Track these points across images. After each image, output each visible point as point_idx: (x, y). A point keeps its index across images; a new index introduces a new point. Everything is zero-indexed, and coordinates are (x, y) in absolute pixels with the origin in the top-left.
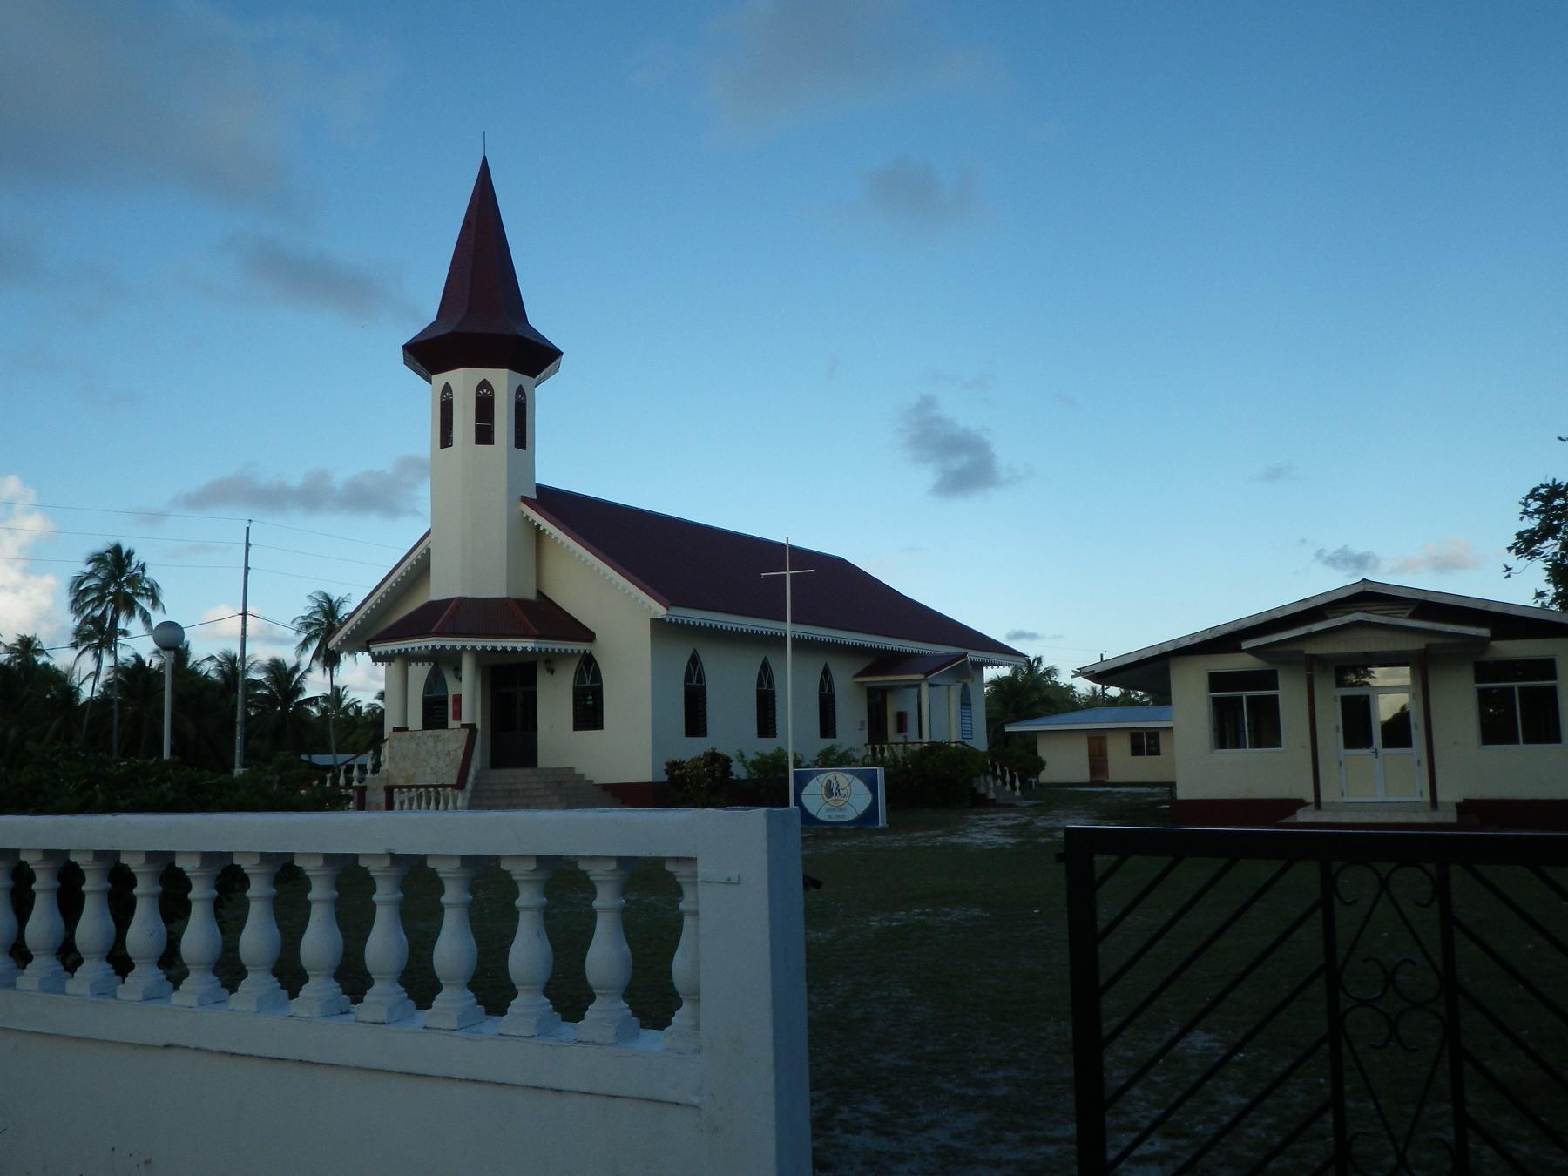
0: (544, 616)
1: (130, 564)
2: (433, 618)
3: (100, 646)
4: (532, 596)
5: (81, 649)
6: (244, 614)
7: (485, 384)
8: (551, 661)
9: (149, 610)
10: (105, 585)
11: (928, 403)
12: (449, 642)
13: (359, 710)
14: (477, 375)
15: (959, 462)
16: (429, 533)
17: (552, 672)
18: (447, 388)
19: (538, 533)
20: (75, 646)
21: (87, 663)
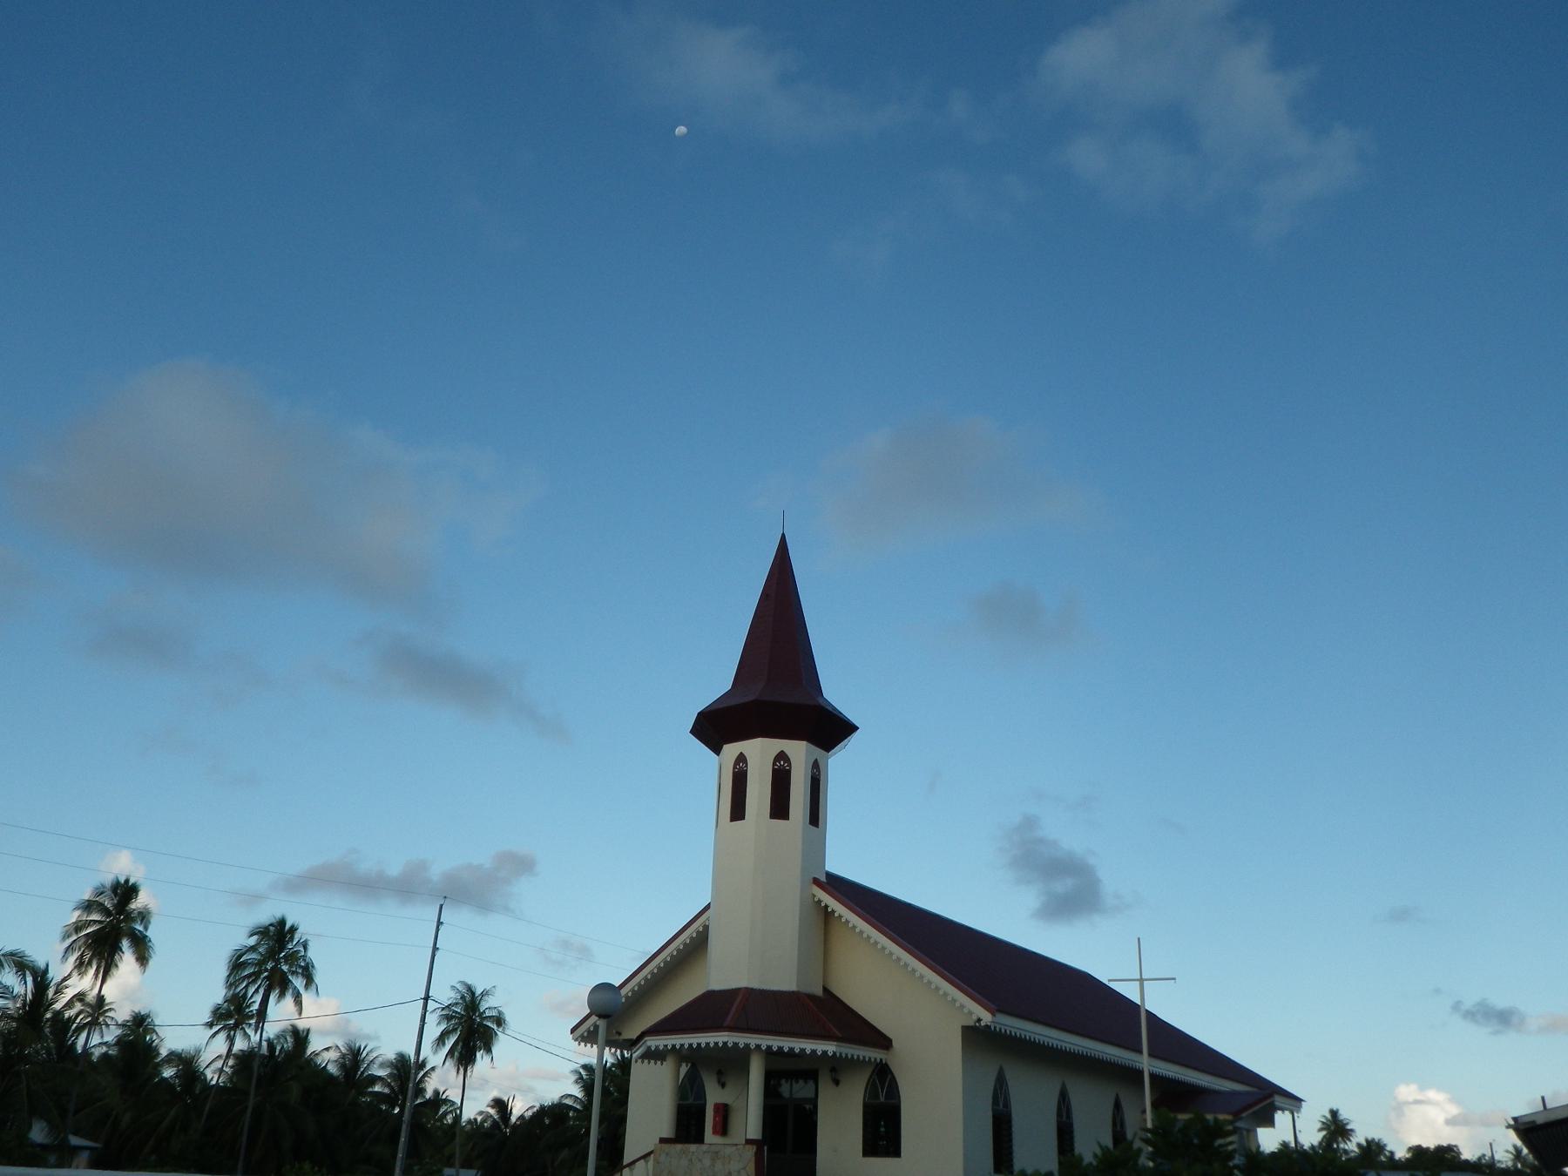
0: (825, 1012)
1: (292, 939)
2: (712, 1010)
3: (236, 1026)
4: (819, 992)
5: (216, 1029)
6: (427, 998)
7: (782, 756)
8: (837, 1068)
9: (302, 990)
10: (261, 963)
11: (1030, 823)
12: (742, 1039)
13: (458, 1118)
14: (774, 745)
15: (1063, 886)
16: (708, 907)
17: (837, 1082)
18: (741, 758)
19: (827, 915)
20: (210, 1025)
21: (220, 1045)
